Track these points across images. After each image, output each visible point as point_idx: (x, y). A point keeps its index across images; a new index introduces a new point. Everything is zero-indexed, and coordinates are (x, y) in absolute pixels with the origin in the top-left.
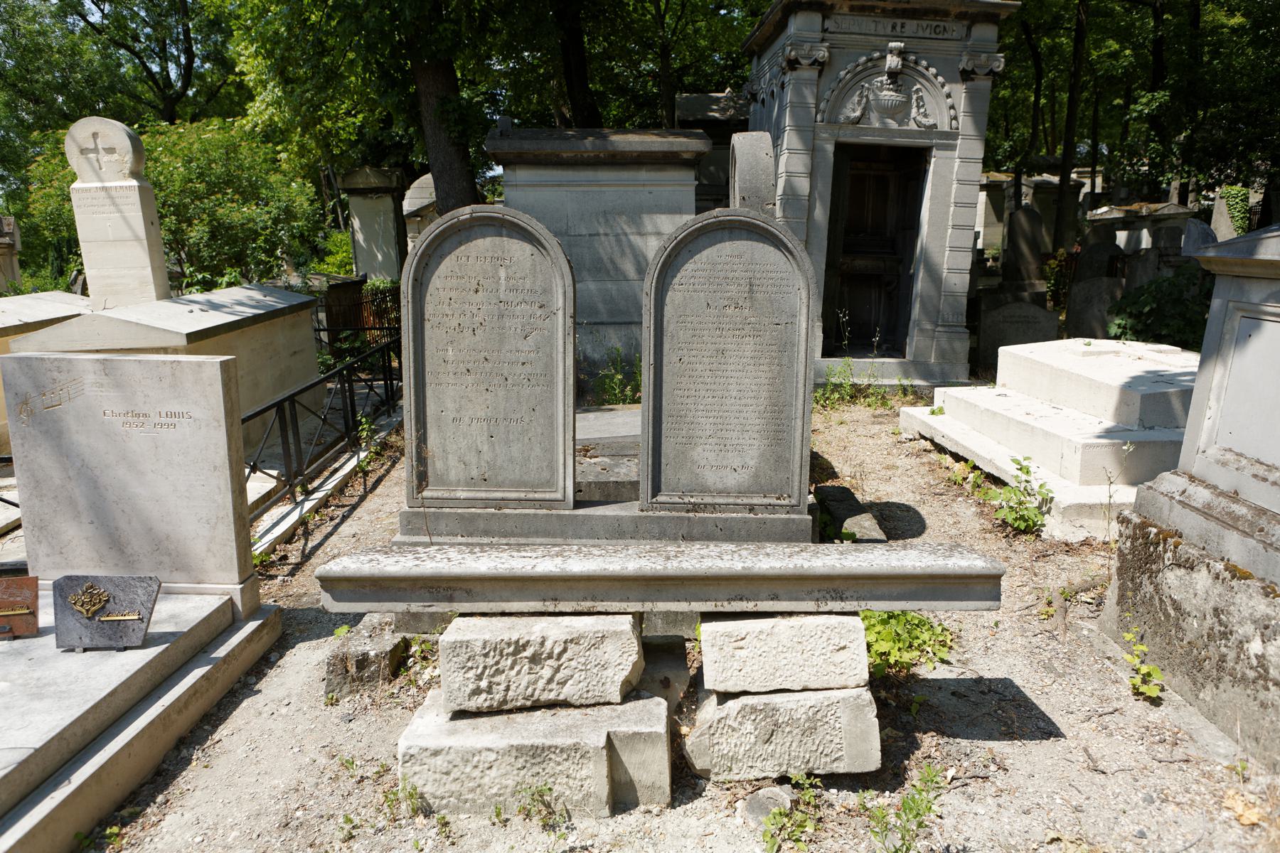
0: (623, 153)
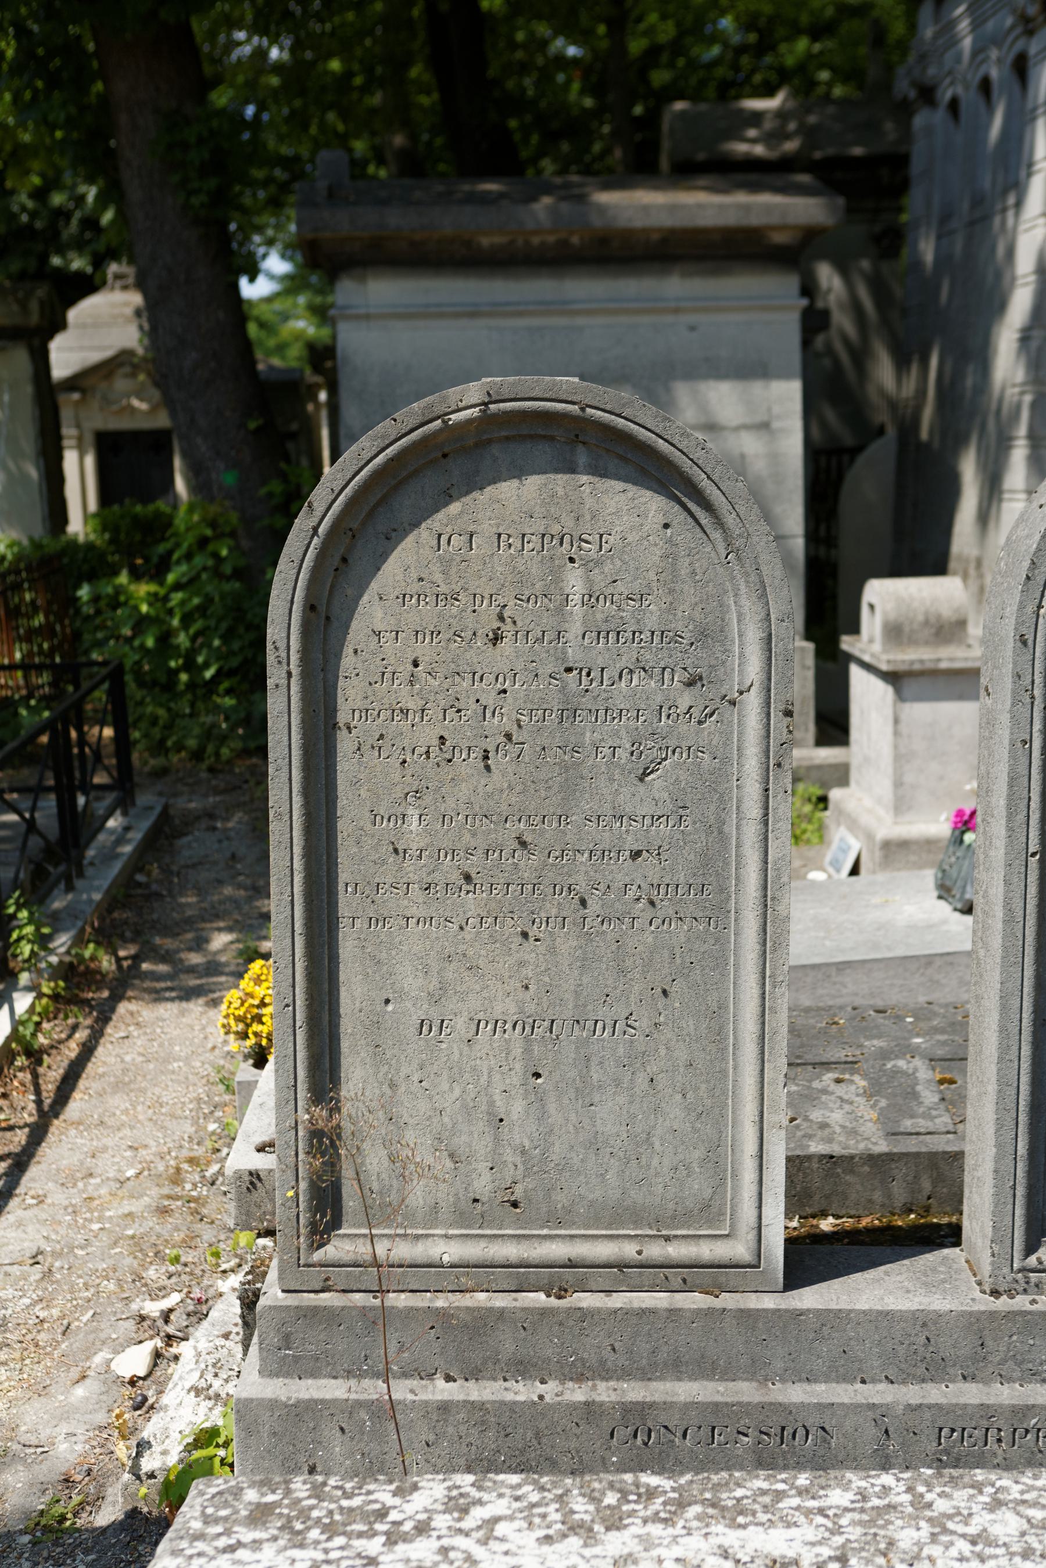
0: (628, 236)
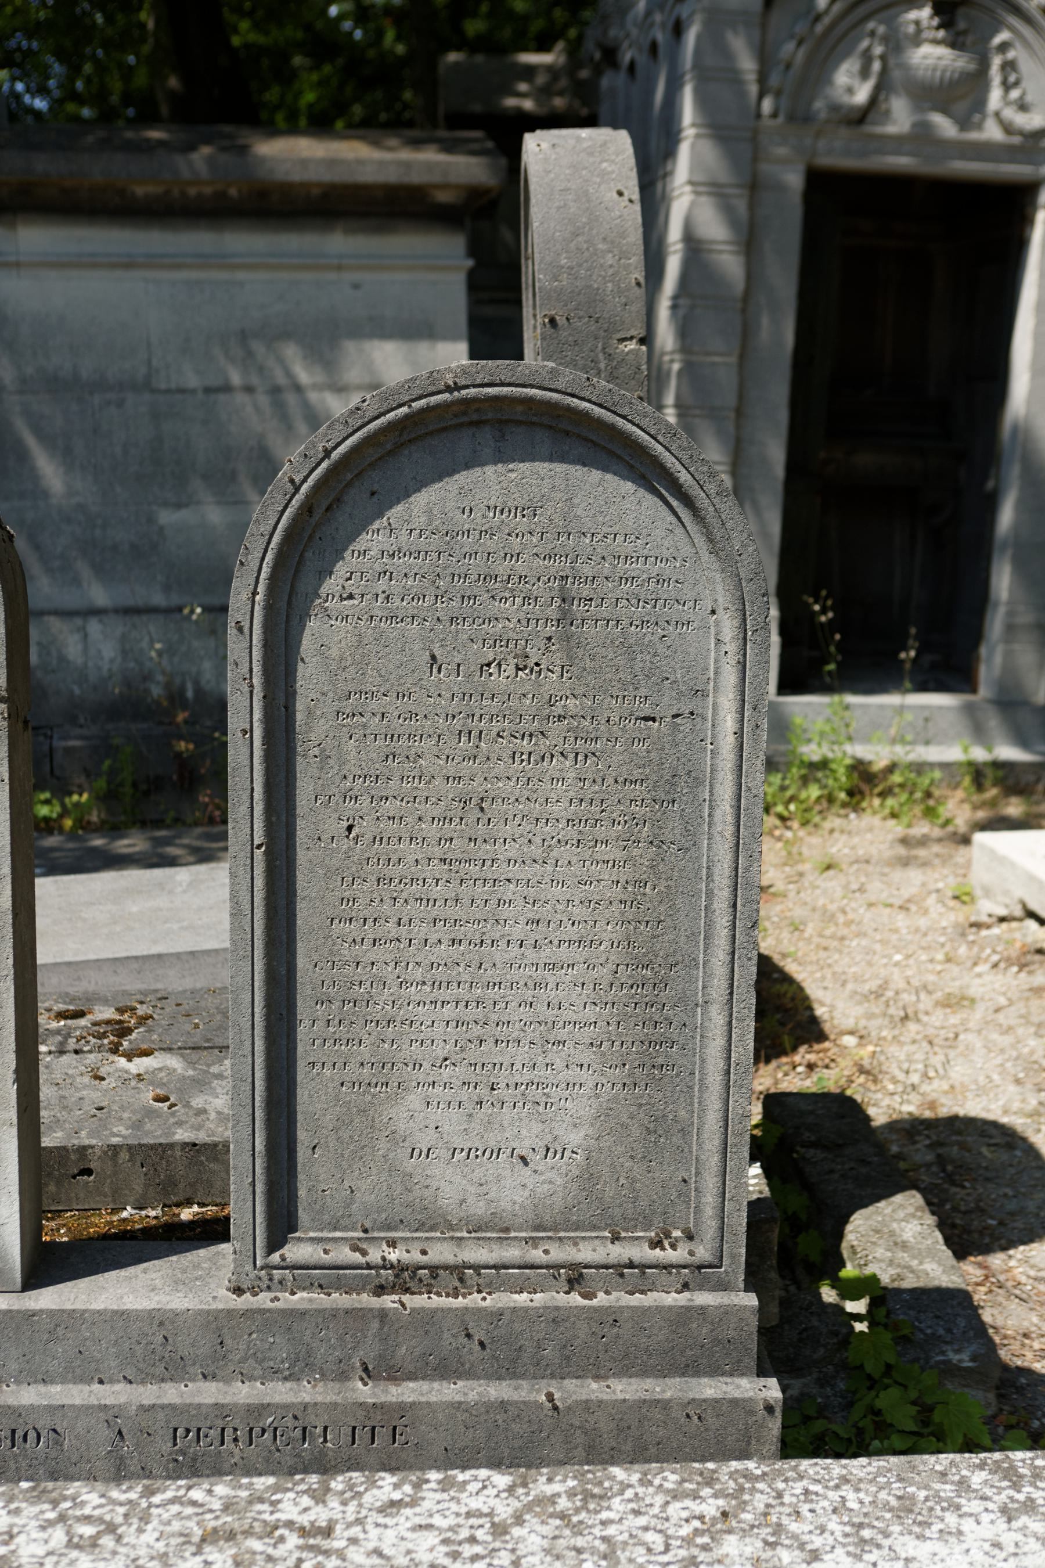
0: (287, 189)
